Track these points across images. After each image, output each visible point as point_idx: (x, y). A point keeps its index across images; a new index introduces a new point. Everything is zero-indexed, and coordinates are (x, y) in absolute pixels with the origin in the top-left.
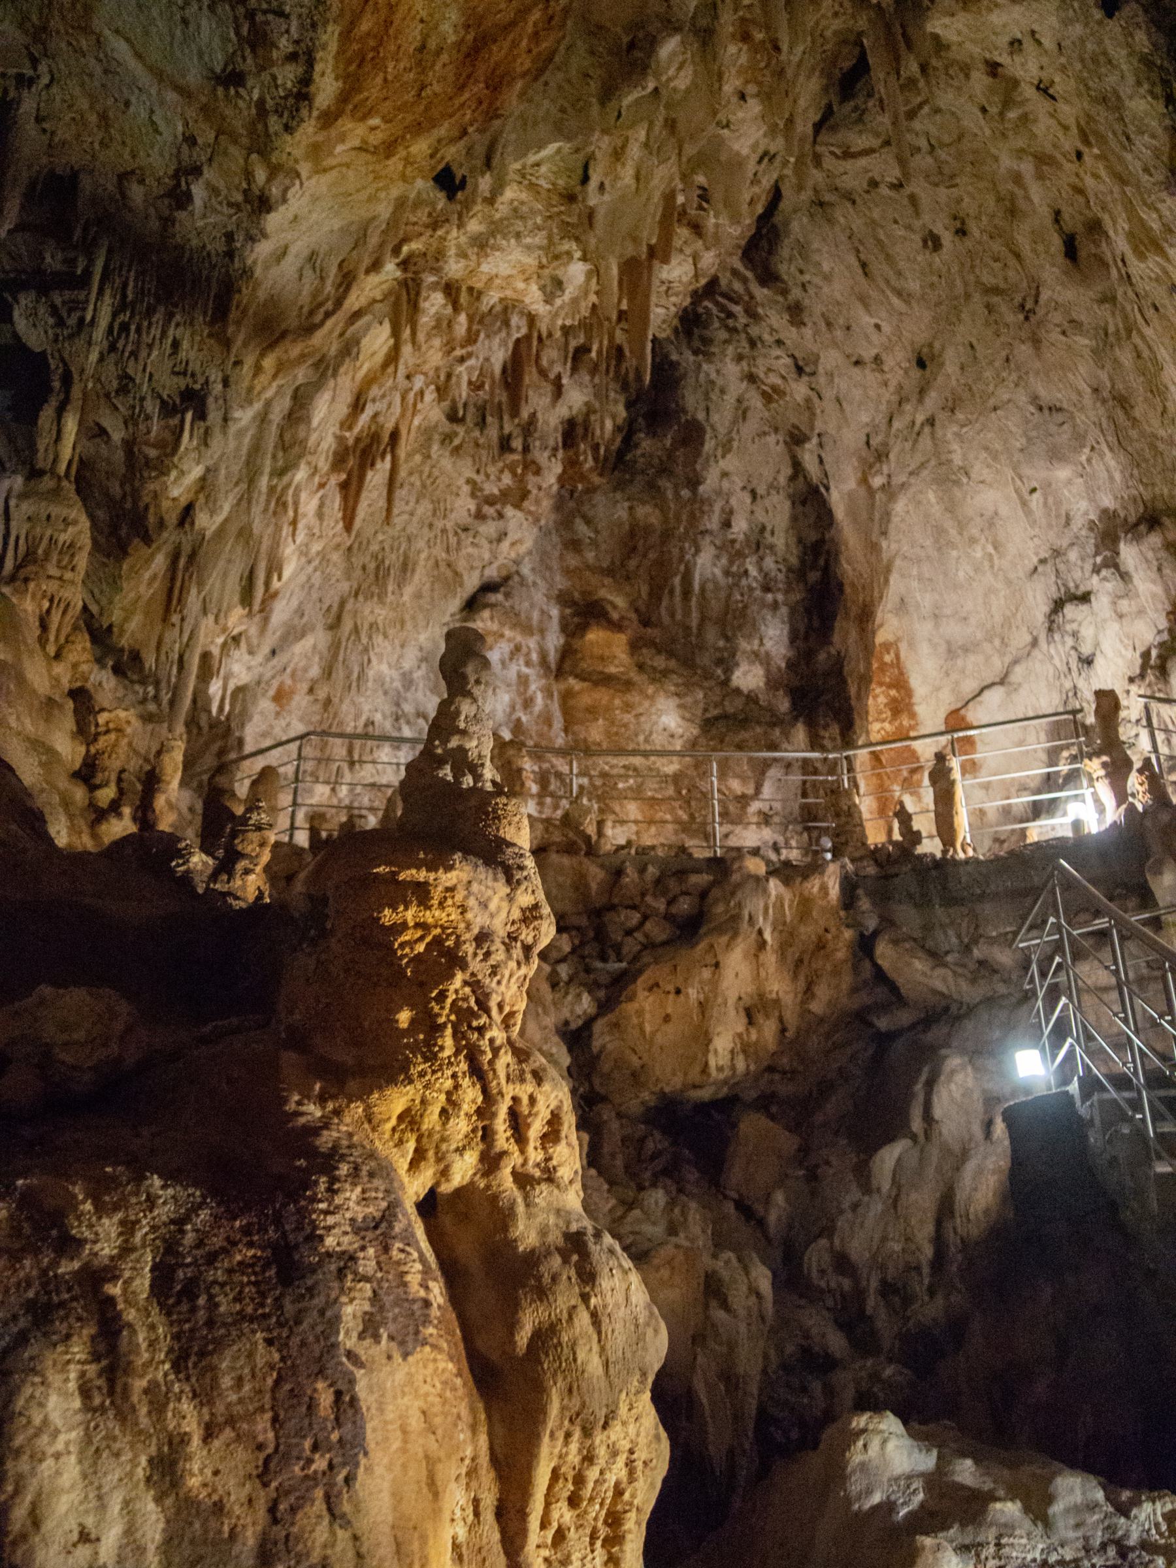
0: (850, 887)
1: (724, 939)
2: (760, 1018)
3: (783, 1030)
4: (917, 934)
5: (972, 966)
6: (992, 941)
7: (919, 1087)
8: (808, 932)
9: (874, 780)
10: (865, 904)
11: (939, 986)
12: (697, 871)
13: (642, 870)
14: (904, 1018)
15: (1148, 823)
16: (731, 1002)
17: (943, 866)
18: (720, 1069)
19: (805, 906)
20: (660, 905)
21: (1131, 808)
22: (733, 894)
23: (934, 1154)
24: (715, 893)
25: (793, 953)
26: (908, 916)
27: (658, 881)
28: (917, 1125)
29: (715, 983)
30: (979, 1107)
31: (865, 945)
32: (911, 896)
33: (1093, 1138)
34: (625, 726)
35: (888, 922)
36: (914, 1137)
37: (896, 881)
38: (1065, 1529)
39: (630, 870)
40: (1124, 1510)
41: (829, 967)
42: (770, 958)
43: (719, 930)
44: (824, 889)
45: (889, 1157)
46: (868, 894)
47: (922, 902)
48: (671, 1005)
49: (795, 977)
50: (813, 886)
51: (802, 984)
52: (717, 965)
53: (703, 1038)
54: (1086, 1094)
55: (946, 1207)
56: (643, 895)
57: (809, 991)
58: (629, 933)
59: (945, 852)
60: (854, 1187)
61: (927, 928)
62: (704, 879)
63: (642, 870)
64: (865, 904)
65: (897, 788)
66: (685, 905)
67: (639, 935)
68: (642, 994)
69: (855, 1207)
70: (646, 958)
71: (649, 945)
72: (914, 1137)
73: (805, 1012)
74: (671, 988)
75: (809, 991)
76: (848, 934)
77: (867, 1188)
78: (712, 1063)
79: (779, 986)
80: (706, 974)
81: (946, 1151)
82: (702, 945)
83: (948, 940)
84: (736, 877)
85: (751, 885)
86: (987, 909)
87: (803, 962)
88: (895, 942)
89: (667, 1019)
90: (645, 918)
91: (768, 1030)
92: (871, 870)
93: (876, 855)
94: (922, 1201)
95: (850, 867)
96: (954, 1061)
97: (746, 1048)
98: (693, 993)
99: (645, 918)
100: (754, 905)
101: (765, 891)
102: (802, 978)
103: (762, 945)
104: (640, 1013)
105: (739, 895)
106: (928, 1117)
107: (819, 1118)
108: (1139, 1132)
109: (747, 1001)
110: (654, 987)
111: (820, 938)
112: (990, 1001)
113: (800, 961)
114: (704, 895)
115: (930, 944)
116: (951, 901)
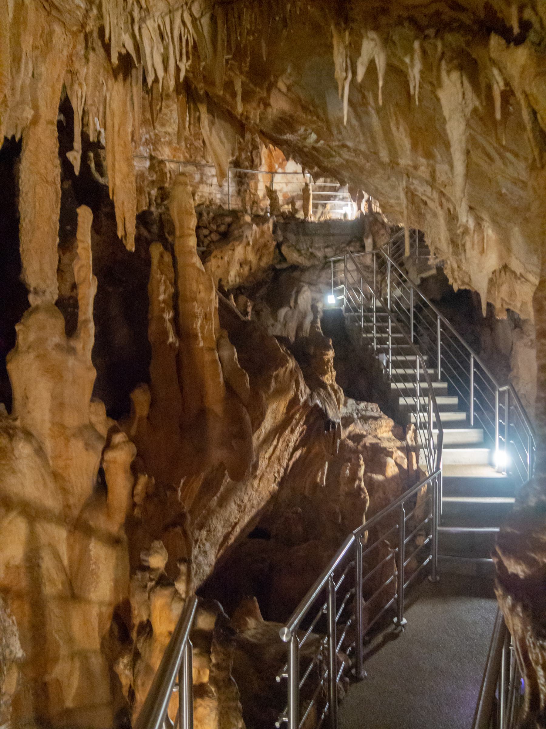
0: (275, 226)
1: (238, 243)
2: (244, 266)
3: (251, 269)
4: (294, 243)
5: (309, 254)
6: (316, 249)
7: (293, 293)
8: (262, 241)
9: (268, 160)
10: (279, 232)
11: (299, 261)
12: (227, 216)
13: (208, 214)
14: (285, 266)
15: (366, 220)
16: (237, 260)
17: (304, 222)
18: (232, 281)
19: (263, 233)
20: (215, 227)
21: (362, 213)
22: (241, 228)
23: (296, 313)
24: (234, 226)
25: (257, 247)
26: (292, 238)
27: (213, 218)
28: (292, 304)
29: (233, 255)
30: (310, 301)
31: (279, 246)
32: (293, 230)
33: (346, 322)
34: (166, 115)
35: (286, 239)
36: (291, 307)
37: (289, 226)
38: (349, 407)
39: (205, 214)
40: (358, 404)
41: (267, 252)
42: (249, 249)
43: (235, 239)
44: (269, 228)
45: (283, 312)
46: (280, 229)
47: (297, 234)
48: (220, 262)
49: (256, 254)
50: (265, 227)
51: (258, 257)
52: (234, 250)
53: (227, 272)
54: (346, 312)
55: (300, 327)
56: (209, 223)
57: (260, 259)
58: (205, 236)
59: (305, 218)
60: (271, 319)
61: (297, 241)
62: (228, 220)
63: (208, 214)
64: (279, 232)
65: (277, 166)
66: (223, 228)
67: (209, 238)
68: (212, 259)
69: (273, 325)
70: (213, 247)
71: (212, 242)
72: (291, 307)
73: (258, 265)
74: (220, 257)
75: (260, 259)
76: (275, 243)
77: (276, 320)
78: (230, 279)
79: (252, 257)
80: (230, 252)
81: (300, 312)
82: (230, 244)
83: (303, 246)
84: (242, 222)
85: (246, 226)
86: (316, 238)
87: (260, 249)
88: (289, 247)
89: (218, 267)
90: (211, 232)
91: (246, 268)
92: (282, 221)
93: (283, 214)
94: (292, 326)
95: (275, 219)
96: (305, 288)
97: (239, 275)
98: (226, 258)
99: (211, 232)
100: (248, 233)
101: (252, 229)
102: (258, 255)
103: (248, 244)
104: (211, 265)
105: (243, 229)
106: (296, 302)
107: (257, 295)
108: (360, 326)
109: (241, 261)
110: (215, 256)
111: (265, 243)
112: (314, 266)
113: (258, 250)
114: (229, 225)
115: (298, 247)
116: (305, 234)
